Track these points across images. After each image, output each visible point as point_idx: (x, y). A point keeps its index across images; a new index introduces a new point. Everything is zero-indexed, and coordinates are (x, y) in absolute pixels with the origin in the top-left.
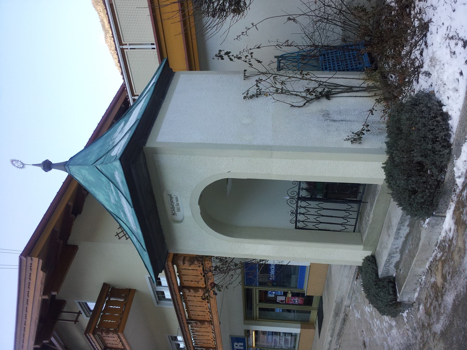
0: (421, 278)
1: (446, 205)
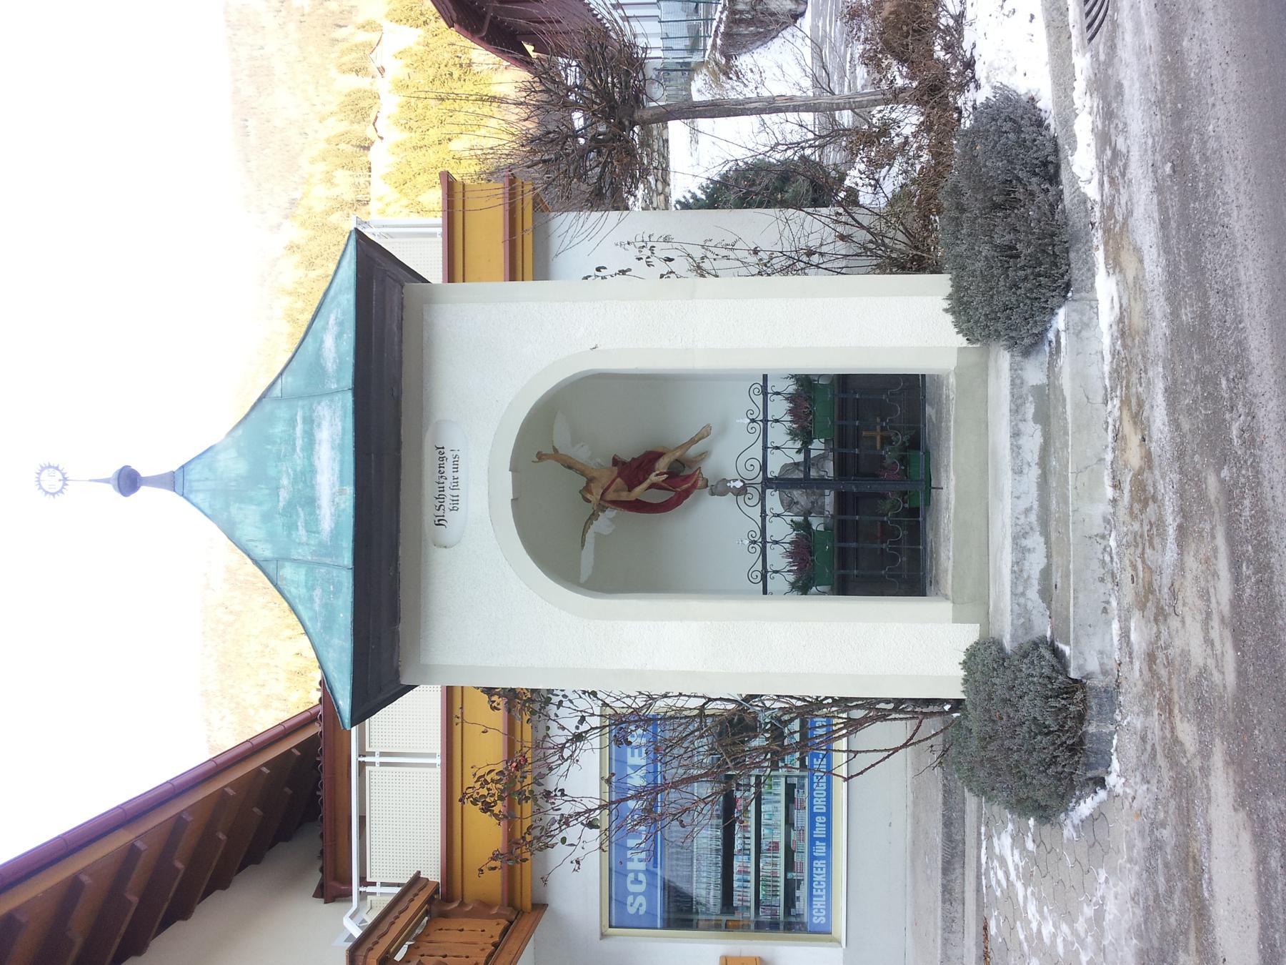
0: (1108, 549)
1: (1089, 270)
